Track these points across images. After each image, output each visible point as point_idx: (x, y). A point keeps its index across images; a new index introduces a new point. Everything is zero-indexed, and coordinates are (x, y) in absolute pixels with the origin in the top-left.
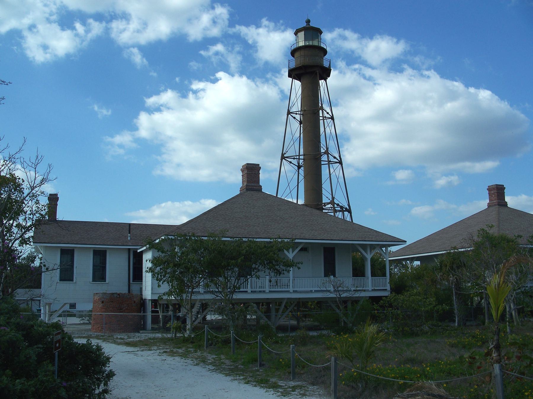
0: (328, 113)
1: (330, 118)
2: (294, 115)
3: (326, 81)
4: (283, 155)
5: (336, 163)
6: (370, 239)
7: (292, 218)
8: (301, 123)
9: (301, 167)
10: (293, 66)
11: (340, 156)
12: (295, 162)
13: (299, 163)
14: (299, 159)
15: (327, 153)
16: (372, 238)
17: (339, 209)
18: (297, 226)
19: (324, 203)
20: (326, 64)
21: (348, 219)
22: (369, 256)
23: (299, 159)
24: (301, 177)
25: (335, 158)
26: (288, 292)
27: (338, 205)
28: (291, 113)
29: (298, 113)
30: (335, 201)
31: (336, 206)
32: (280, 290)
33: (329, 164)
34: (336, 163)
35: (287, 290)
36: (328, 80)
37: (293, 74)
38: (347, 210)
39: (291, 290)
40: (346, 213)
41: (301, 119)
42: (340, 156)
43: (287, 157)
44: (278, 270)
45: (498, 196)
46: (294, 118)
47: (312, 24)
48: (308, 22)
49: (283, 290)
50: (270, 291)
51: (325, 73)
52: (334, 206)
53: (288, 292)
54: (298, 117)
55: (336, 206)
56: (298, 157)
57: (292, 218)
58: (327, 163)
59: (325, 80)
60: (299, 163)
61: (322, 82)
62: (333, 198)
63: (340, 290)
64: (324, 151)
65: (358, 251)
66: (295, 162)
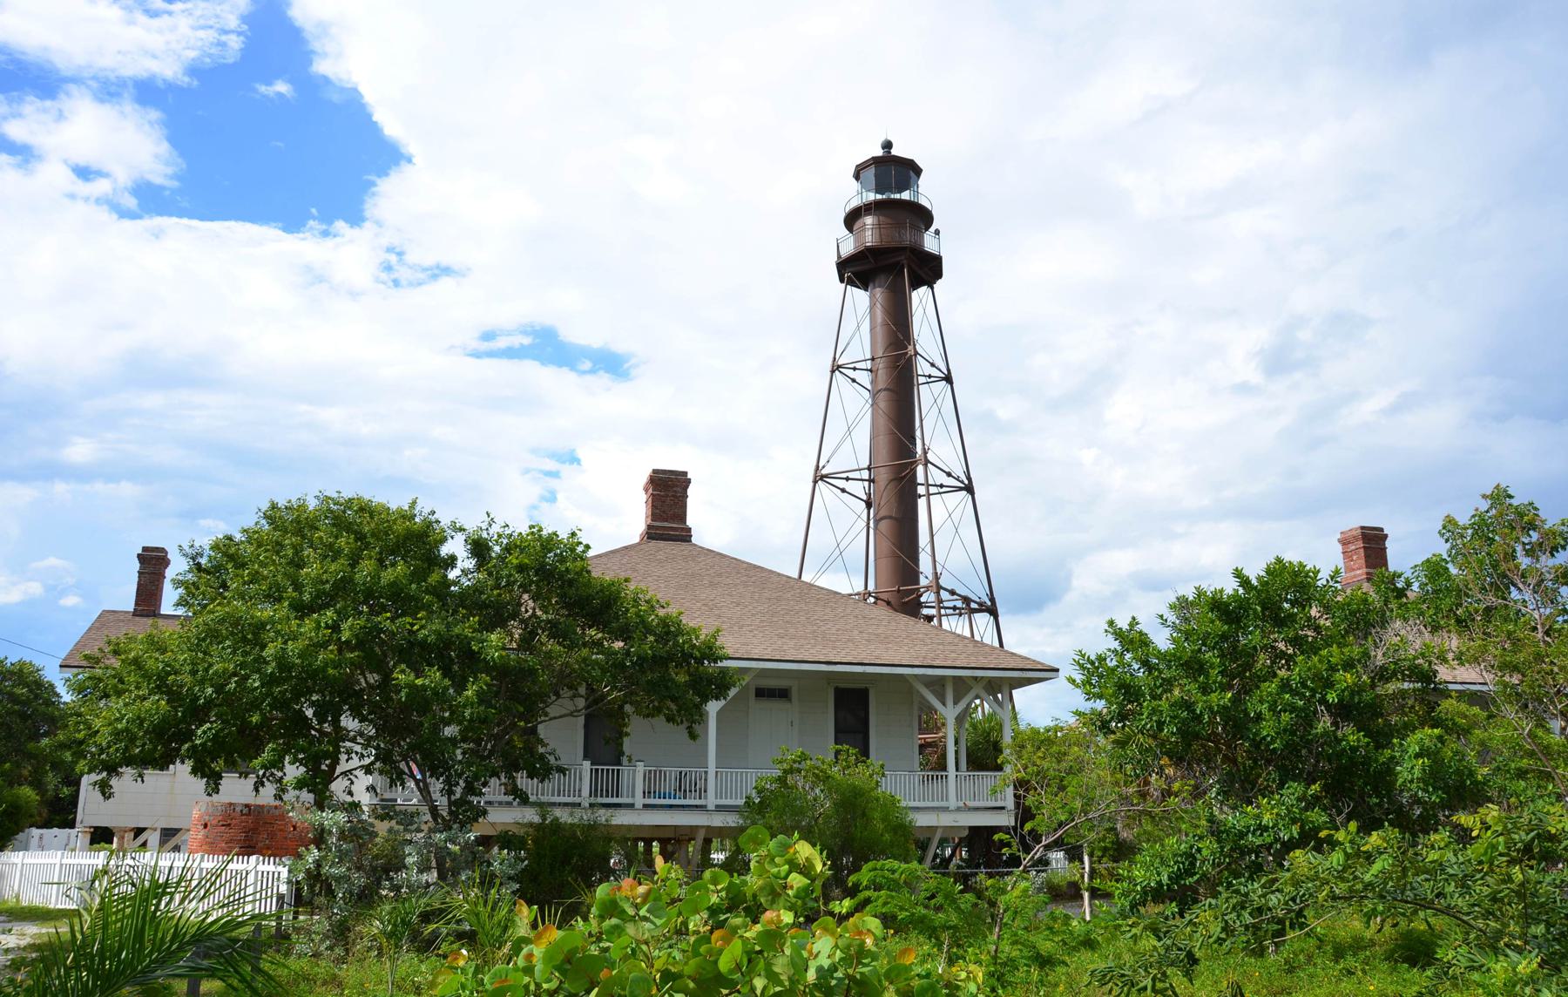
12: (859, 489)
21: (990, 638)
26: (945, 809)
35: (698, 802)
36: (938, 285)
37: (856, 270)
38: (982, 608)
40: (982, 620)
45: (1367, 556)
47: (894, 152)
48: (888, 145)
49: (687, 802)
50: (645, 806)
51: (928, 269)
53: (945, 809)
54: (865, 378)
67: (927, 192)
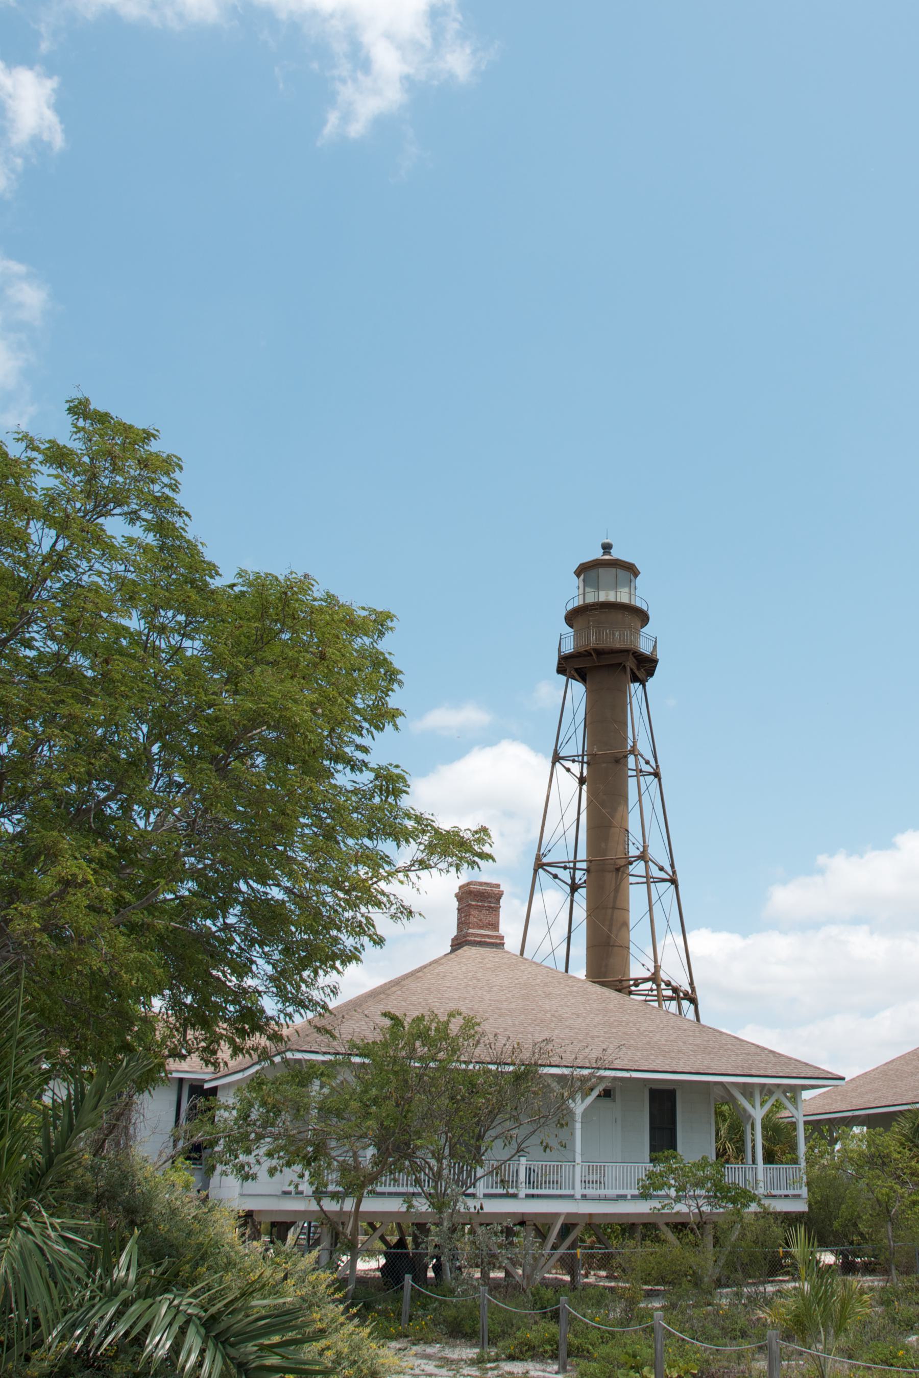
0: (647, 762)
1: (650, 774)
2: (568, 764)
3: (644, 686)
4: (538, 858)
5: (664, 880)
6: (762, 1072)
7: (578, 1016)
8: (582, 781)
9: (580, 887)
10: (569, 647)
11: (672, 866)
12: (565, 875)
13: (573, 879)
14: (575, 869)
15: (643, 857)
16: (766, 1069)
17: (669, 993)
18: (592, 1038)
19: (636, 980)
20: (645, 647)
21: (691, 1015)
22: (758, 1113)
23: (575, 869)
24: (581, 913)
25: (661, 869)
27: (668, 984)
28: (563, 758)
29: (576, 758)
30: (663, 975)
31: (663, 986)
32: (559, 1192)
33: (648, 883)
34: (664, 880)
36: (651, 683)
37: (570, 666)
39: (578, 1191)
40: (685, 1004)
41: (582, 773)
42: (672, 866)
43: (549, 865)
44: (102, 1147)
46: (568, 770)
48: (607, 548)
52: (658, 986)
53: (571, 1197)
55: (663, 986)
56: (571, 865)
57: (578, 1016)
58: (644, 880)
59: (643, 683)
60: (573, 879)
61: (635, 687)
62: (657, 968)
63: (700, 1196)
64: (637, 853)
65: (733, 1099)
66: (565, 875)
67: (643, 593)
